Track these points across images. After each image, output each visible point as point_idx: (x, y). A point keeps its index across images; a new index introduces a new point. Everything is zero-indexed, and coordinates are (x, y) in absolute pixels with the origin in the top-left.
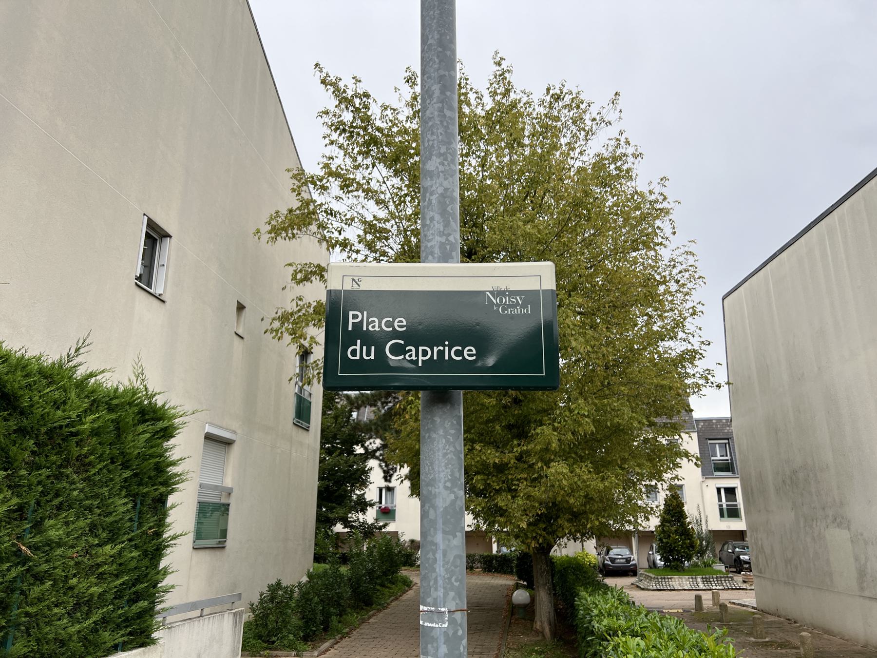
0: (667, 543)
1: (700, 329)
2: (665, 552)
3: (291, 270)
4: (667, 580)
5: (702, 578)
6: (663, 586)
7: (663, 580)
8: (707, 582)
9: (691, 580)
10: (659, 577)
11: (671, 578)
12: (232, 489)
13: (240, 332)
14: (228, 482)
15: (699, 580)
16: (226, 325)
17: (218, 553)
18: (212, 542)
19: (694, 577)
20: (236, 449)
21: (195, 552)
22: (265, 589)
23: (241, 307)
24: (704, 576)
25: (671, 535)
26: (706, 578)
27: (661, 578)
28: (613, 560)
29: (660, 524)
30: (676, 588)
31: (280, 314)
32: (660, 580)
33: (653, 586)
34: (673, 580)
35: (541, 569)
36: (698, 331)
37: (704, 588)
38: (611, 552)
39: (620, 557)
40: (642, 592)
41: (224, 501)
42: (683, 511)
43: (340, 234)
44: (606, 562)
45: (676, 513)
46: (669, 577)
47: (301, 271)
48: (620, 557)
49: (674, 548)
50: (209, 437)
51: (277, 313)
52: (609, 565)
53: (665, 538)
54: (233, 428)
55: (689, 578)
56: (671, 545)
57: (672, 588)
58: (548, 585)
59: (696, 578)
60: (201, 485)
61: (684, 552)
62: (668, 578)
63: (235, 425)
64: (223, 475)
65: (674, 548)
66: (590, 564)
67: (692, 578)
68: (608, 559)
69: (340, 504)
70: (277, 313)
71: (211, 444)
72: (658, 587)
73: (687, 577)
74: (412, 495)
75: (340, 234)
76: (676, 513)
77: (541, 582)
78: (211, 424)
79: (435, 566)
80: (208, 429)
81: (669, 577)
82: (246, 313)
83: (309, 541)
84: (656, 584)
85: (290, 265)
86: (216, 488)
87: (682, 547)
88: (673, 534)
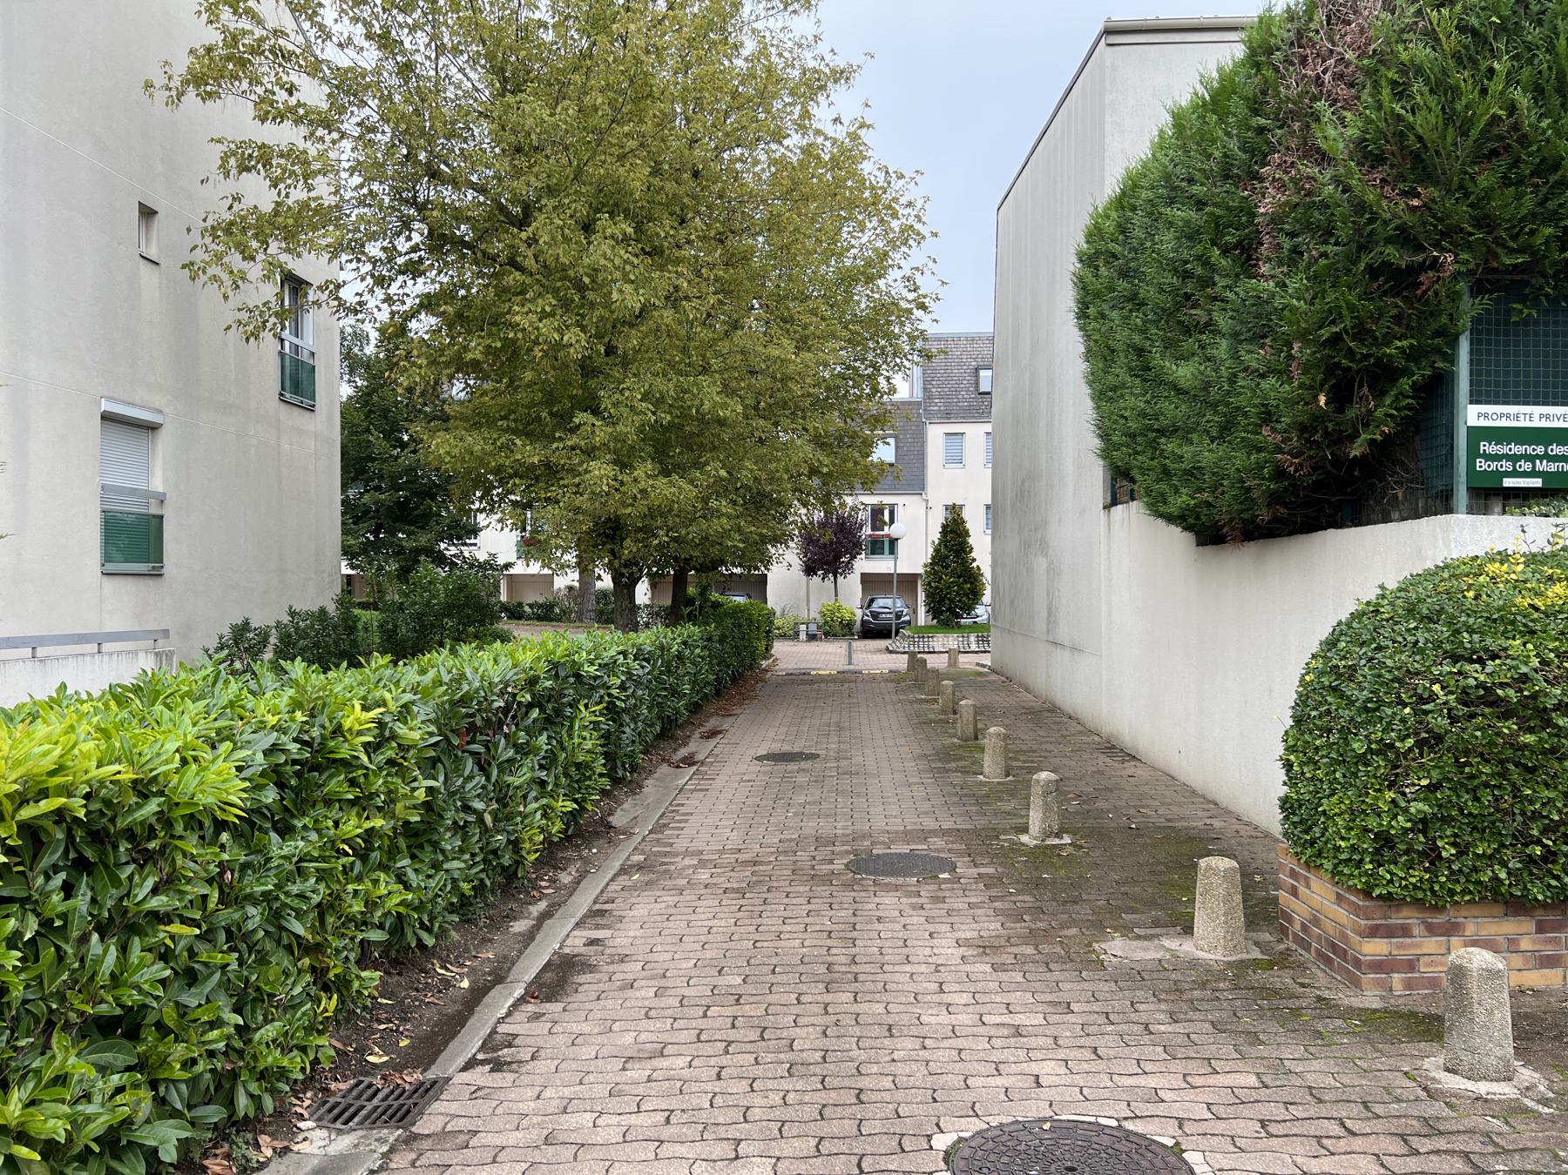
0: (937, 588)
1: (935, 261)
3: (221, 148)
12: (165, 494)
13: (153, 253)
14: (158, 484)
15: (973, 638)
16: (119, 244)
17: (150, 582)
18: (143, 567)
20: (164, 437)
21: (107, 581)
22: (227, 631)
23: (147, 213)
28: (875, 615)
31: (210, 222)
36: (931, 264)
38: (874, 605)
41: (154, 510)
43: (291, 94)
47: (234, 154)
50: (107, 418)
51: (205, 220)
54: (157, 405)
60: (103, 487)
63: (159, 400)
64: (148, 469)
69: (423, 528)
70: (205, 220)
71: (117, 431)
75: (291, 94)
78: (109, 398)
79: (929, 666)
80: (105, 406)
82: (158, 222)
83: (330, 575)
85: (219, 141)
86: (133, 492)
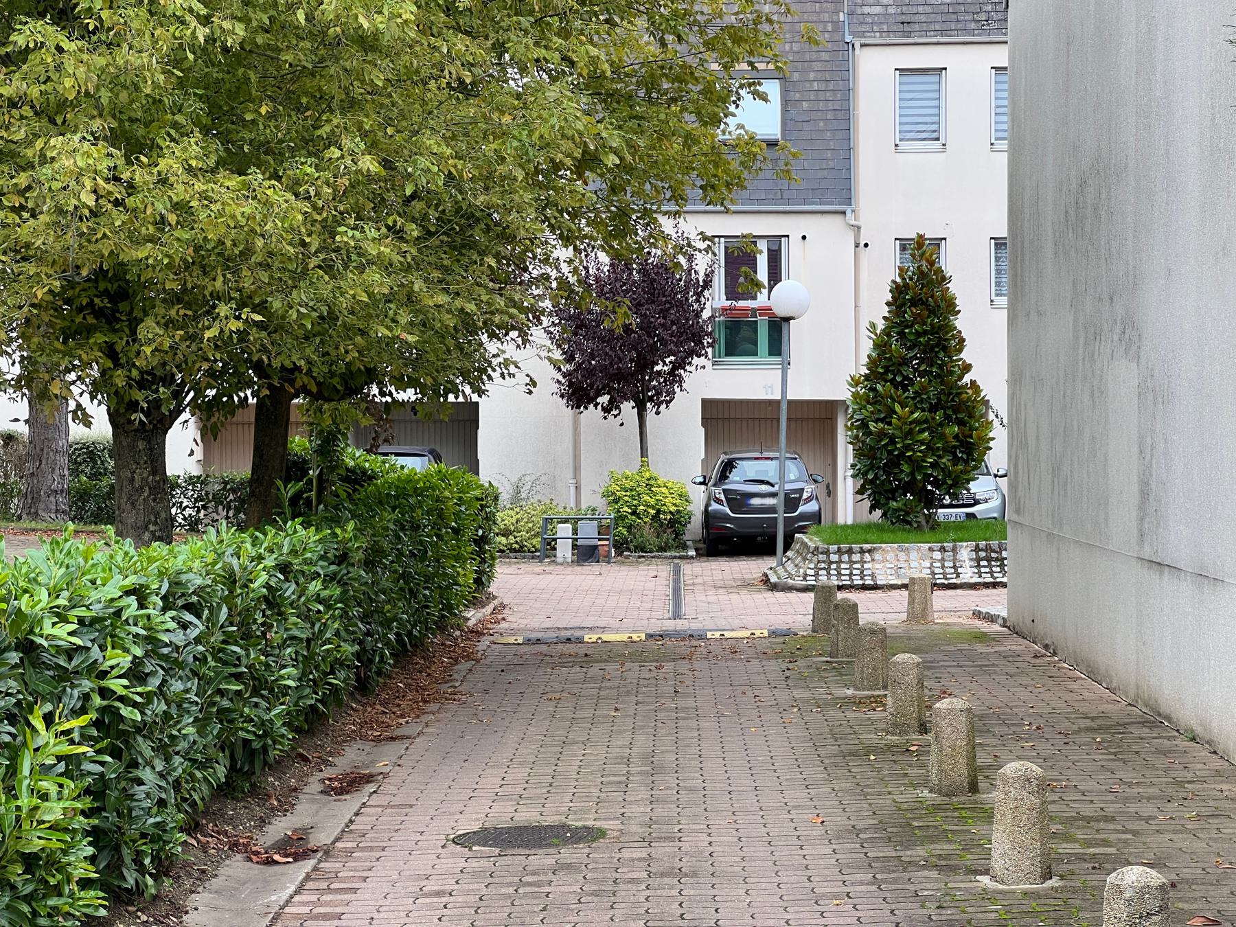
0: (882, 434)
2: (872, 467)
4: (856, 557)
5: (977, 549)
6: (839, 574)
7: (845, 557)
8: (989, 559)
9: (937, 555)
10: (834, 548)
11: (869, 551)
19: (948, 545)
24: (982, 544)
25: (898, 408)
26: (988, 549)
27: (839, 551)
28: (738, 501)
29: (864, 371)
30: (881, 581)
32: (834, 558)
33: (805, 576)
34: (877, 556)
35: (132, 480)
37: (976, 580)
38: (735, 476)
39: (764, 488)
40: (780, 595)
42: (951, 328)
44: (715, 506)
45: (925, 333)
46: (867, 546)
48: (764, 488)
49: (902, 454)
52: (727, 518)
53: (876, 421)
55: (931, 549)
56: (892, 441)
57: (869, 582)
58: (152, 528)
59: (954, 550)
61: (934, 465)
62: (862, 551)
65: (902, 454)
66: (659, 511)
67: (943, 549)
68: (722, 497)
72: (823, 578)
73: (927, 546)
74: (787, 320)
76: (925, 333)
77: (131, 521)
81: (867, 546)
84: (817, 569)
87: (930, 449)
88: (903, 406)
